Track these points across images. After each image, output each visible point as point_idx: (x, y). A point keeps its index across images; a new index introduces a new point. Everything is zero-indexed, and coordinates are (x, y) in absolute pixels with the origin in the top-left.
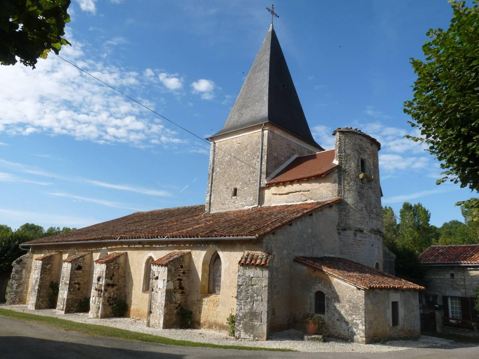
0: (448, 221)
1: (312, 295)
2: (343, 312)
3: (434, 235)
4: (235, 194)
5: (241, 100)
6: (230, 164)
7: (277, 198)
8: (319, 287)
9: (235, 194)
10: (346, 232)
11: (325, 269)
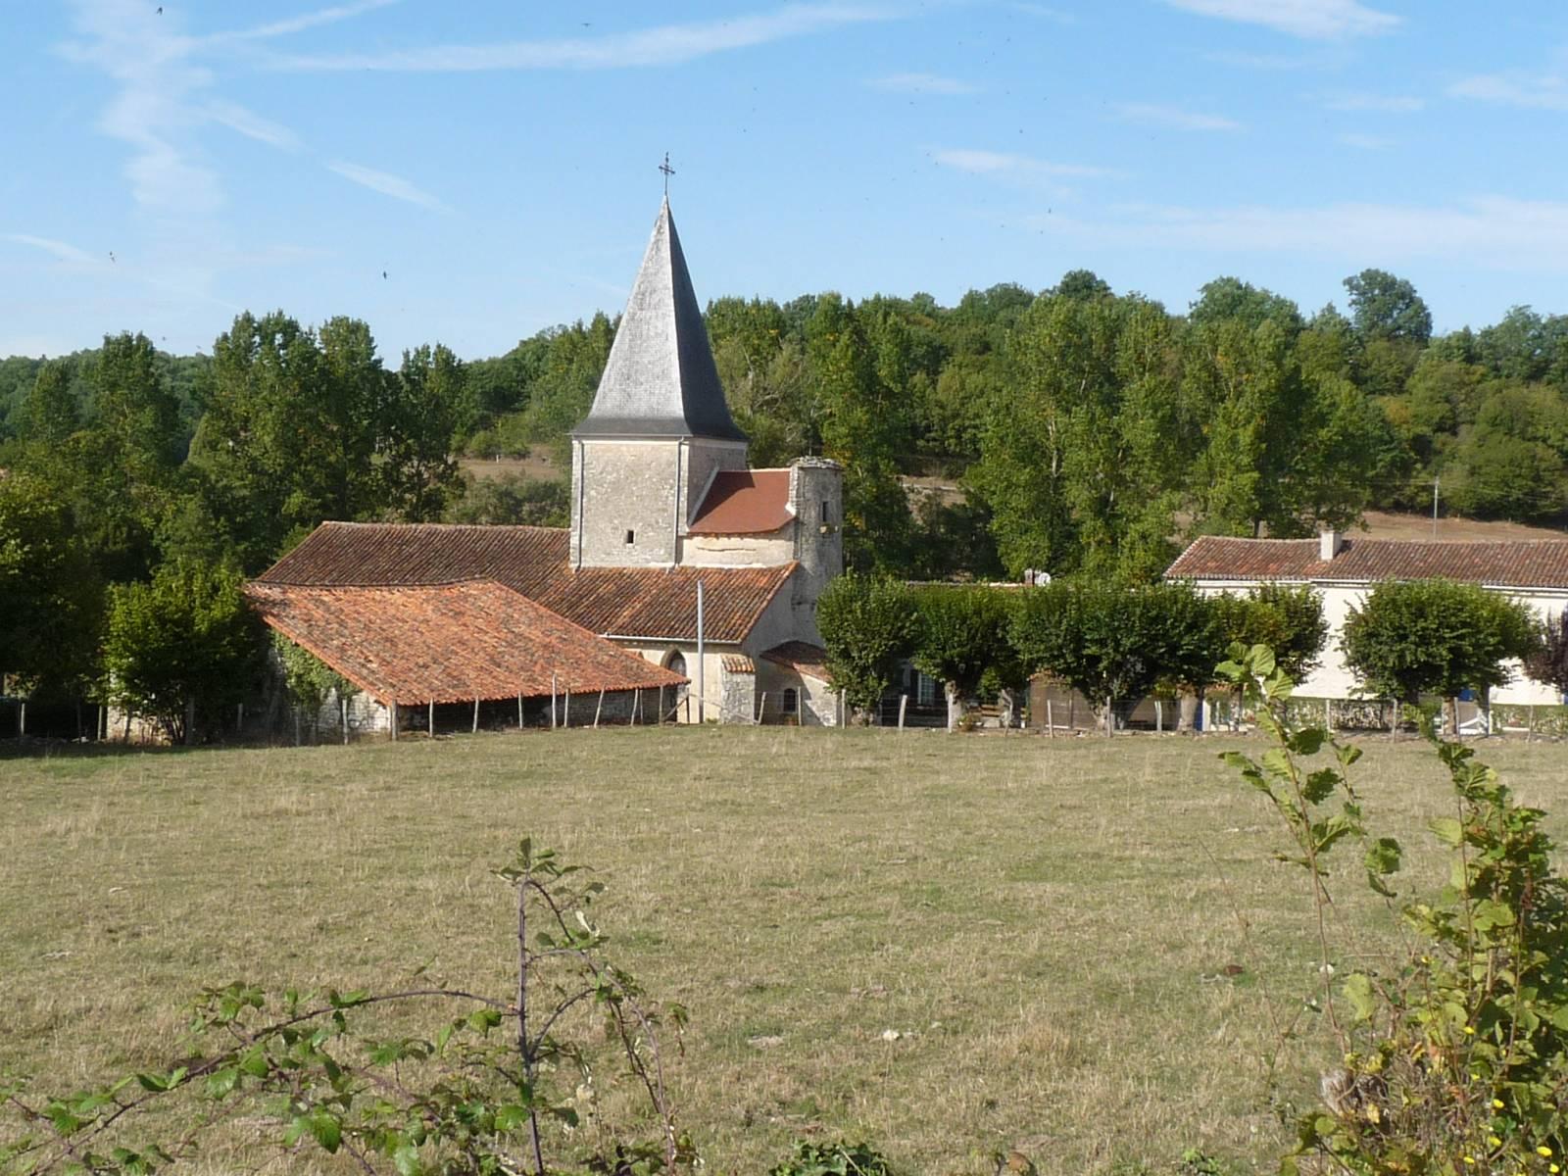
0: (983, 286)
1: (782, 693)
2: (814, 709)
3: (923, 357)
4: (630, 538)
5: (620, 363)
6: (616, 487)
7: (706, 554)
8: (789, 685)
9: (630, 538)
10: (802, 607)
11: (796, 666)
